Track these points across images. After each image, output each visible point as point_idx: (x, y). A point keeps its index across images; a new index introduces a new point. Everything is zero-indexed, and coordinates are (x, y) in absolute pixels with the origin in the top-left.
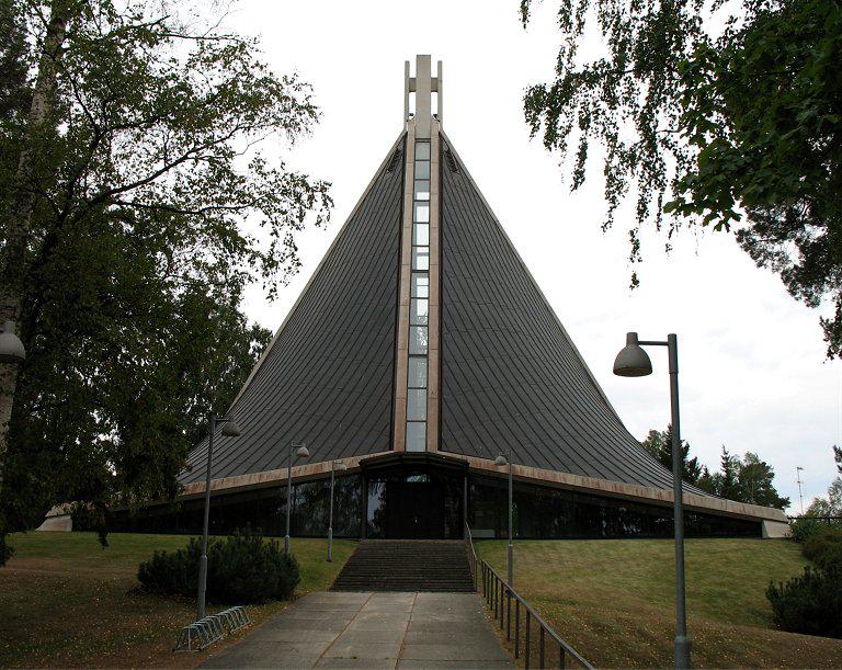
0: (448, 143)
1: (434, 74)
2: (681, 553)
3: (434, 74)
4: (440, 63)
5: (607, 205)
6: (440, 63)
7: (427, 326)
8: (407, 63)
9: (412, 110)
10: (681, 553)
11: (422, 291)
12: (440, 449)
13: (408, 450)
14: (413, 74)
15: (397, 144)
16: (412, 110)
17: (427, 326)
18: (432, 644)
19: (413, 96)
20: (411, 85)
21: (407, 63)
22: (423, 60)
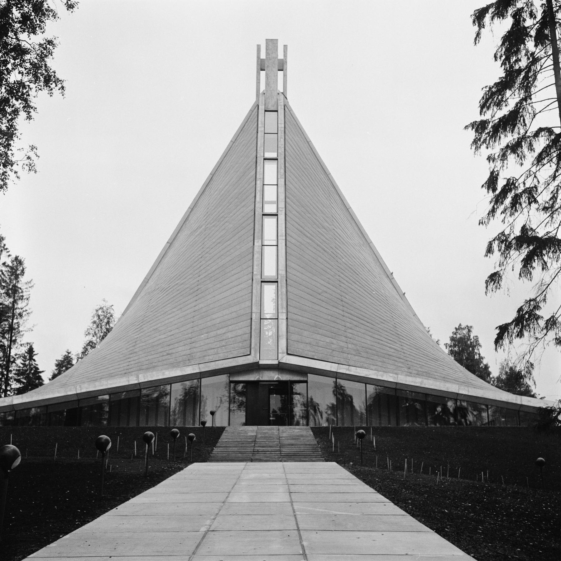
0: (290, 110)
1: (281, 56)
2: (78, 405)
3: (281, 56)
4: (285, 47)
5: (476, 28)
6: (285, 47)
7: (277, 185)
8: (259, 47)
9: (263, 88)
10: (78, 405)
11: (270, 194)
12: (145, 379)
13: (556, 97)
14: (263, 56)
15: (251, 111)
16: (263, 88)
17: (277, 185)
18: (265, 105)
19: (263, 73)
20: (261, 67)
21: (259, 47)
22: (272, 44)
